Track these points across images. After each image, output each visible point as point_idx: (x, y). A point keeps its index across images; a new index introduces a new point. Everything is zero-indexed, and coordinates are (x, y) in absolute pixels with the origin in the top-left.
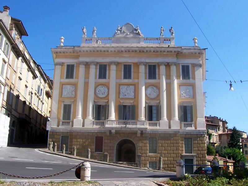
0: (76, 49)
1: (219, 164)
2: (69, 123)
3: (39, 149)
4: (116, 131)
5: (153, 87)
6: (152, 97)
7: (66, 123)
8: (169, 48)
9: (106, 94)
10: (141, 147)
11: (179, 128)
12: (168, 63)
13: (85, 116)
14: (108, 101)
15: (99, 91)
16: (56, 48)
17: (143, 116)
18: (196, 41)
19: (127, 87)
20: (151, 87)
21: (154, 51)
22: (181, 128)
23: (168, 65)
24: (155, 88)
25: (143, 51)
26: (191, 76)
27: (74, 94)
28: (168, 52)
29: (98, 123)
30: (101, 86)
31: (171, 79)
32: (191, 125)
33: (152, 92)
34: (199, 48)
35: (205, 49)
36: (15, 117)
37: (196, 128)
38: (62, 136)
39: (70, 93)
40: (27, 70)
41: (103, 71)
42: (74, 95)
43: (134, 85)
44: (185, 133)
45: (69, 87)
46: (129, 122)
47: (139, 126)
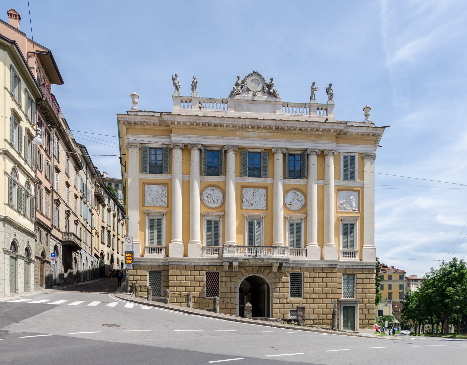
2: (161, 250)
5: (296, 192)
7: (156, 251)
13: (322, 244)
19: (254, 190)
20: (293, 191)
22: (339, 259)
23: (322, 155)
24: (299, 193)
28: (324, 130)
30: (211, 188)
33: (295, 200)
39: (159, 200)
44: (344, 267)
45: (155, 187)
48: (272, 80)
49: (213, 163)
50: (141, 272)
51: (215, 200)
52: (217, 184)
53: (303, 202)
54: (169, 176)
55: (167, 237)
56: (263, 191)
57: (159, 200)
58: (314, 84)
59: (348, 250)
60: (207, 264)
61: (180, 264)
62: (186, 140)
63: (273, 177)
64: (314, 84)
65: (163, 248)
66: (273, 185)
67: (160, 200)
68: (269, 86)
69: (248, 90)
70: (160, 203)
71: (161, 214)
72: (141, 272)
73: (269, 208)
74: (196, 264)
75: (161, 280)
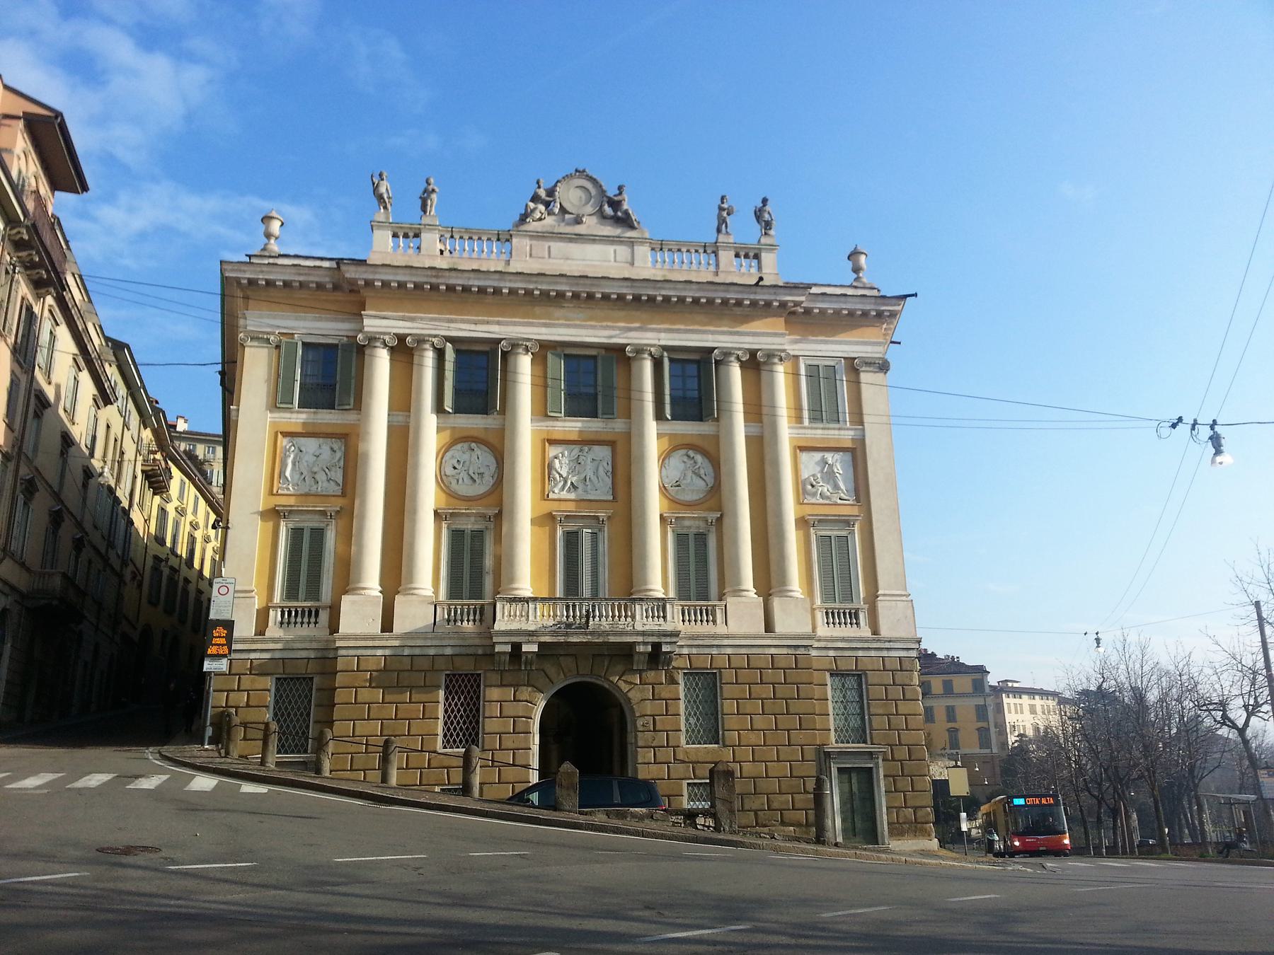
0: (351, 272)
3: (169, 750)
4: (541, 645)
5: (691, 453)
6: (689, 497)
8: (759, 289)
9: (488, 481)
11: (808, 629)
12: (401, 338)
14: (500, 512)
16: (247, 259)
17: (658, 575)
20: (683, 452)
21: (576, 296)
24: (699, 458)
26: (845, 406)
27: (340, 481)
29: (310, 612)
30: (466, 445)
32: (857, 617)
33: (690, 474)
34: (875, 293)
35: (906, 297)
36: (13, 588)
37: (875, 632)
38: (447, 675)
39: (321, 477)
40: (71, 361)
41: (477, 381)
43: (612, 444)
46: (574, 606)
47: (642, 621)
51: (475, 477)
52: (482, 435)
53: (710, 481)
54: (351, 417)
56: (603, 453)
57: (321, 477)
59: (843, 606)
60: (448, 651)
61: (369, 652)
62: (402, 327)
65: (324, 608)
67: (324, 478)
68: (615, 205)
71: (323, 513)
73: (620, 495)
74: (417, 651)
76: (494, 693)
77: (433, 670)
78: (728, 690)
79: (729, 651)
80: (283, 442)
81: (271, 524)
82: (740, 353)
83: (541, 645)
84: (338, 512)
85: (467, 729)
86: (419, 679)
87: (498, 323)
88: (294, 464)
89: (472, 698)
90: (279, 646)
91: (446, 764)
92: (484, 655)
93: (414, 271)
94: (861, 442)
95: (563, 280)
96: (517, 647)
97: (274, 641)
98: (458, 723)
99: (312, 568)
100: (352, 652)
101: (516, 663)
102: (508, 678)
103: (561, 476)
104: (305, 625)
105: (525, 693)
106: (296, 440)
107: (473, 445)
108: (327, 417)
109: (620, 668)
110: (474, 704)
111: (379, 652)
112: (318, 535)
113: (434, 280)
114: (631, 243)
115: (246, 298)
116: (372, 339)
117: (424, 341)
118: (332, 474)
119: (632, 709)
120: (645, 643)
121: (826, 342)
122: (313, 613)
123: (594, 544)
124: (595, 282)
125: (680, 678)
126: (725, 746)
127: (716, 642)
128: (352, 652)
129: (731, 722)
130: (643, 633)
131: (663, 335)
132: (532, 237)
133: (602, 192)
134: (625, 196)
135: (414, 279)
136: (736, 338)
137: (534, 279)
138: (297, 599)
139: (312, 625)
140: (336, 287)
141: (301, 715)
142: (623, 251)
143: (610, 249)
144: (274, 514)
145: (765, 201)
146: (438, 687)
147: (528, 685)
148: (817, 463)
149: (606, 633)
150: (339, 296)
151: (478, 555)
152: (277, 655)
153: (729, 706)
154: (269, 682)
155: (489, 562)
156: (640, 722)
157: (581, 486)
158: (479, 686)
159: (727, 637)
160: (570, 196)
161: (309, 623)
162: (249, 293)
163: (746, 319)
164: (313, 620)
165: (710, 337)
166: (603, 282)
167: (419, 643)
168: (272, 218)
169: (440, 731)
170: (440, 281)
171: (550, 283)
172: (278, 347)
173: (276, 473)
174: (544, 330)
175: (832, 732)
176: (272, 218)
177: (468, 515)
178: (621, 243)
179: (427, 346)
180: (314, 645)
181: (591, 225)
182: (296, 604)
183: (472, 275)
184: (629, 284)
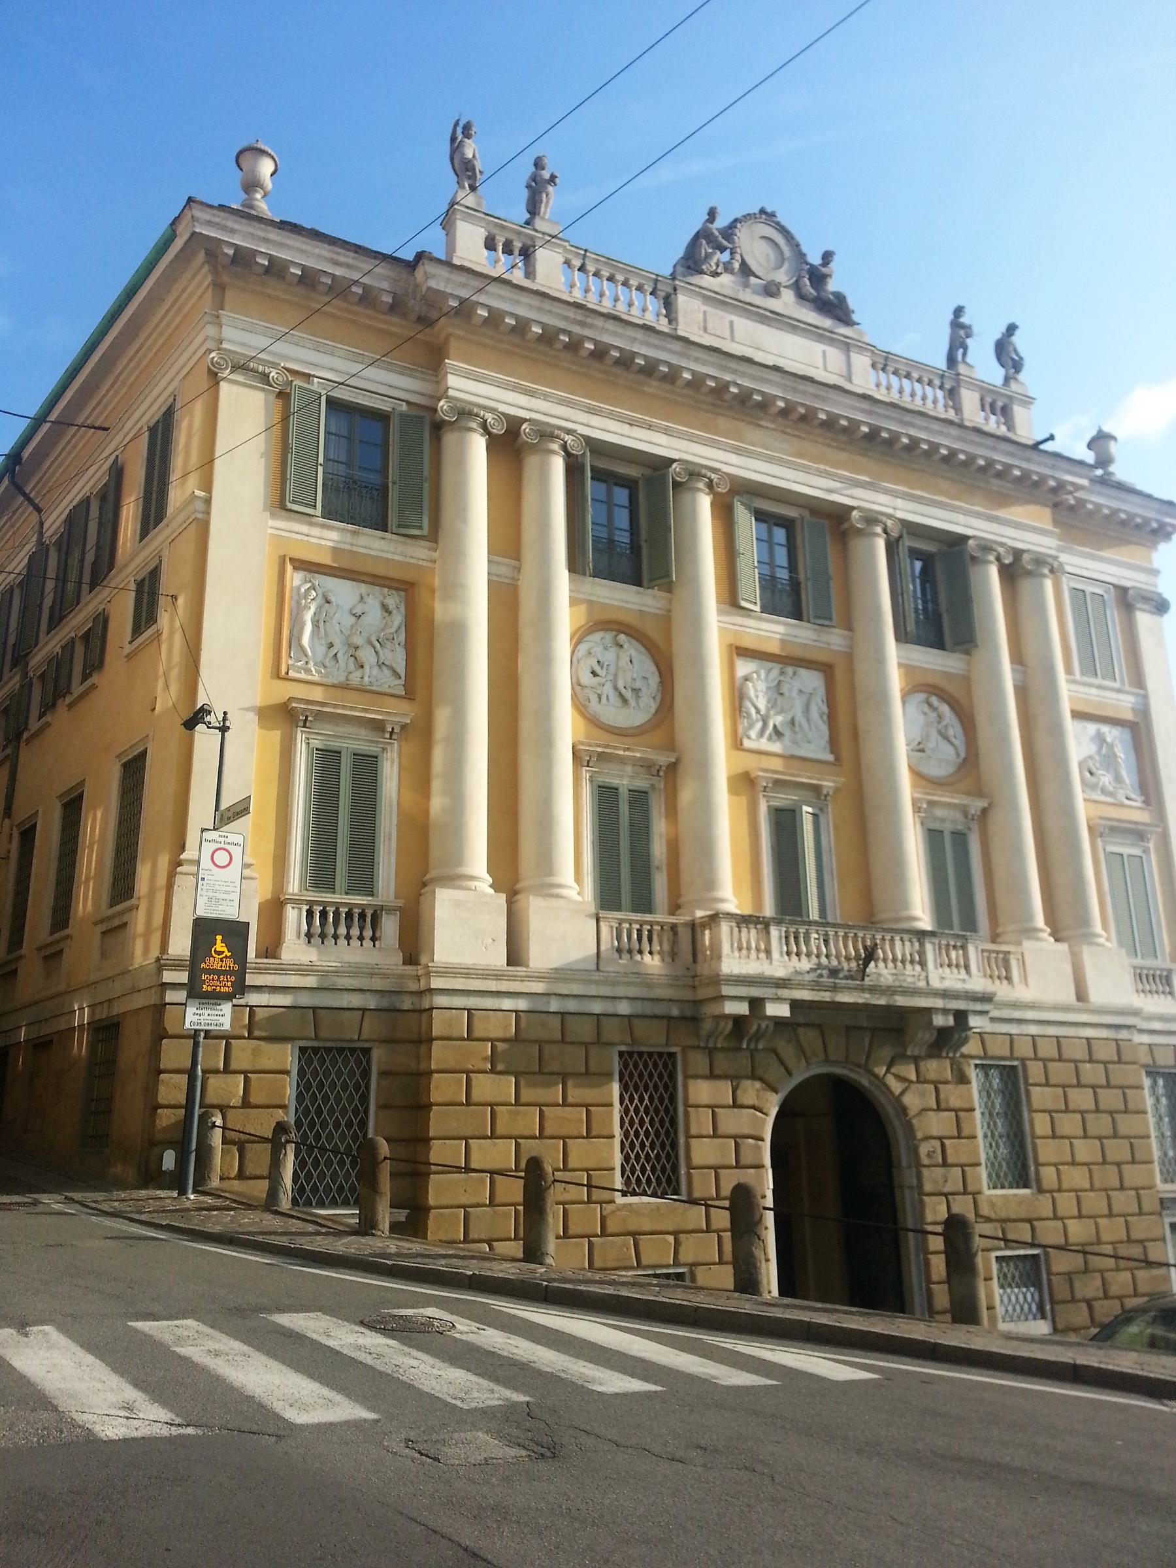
1: (522, 1181)
4: (795, 1004)
5: (934, 700)
8: (1034, 455)
10: (937, 1144)
12: (514, 425)
13: (512, 872)
15: (594, 673)
18: (266, 167)
19: (782, 673)
24: (945, 709)
25: (574, 346)
27: (401, 670)
29: (362, 916)
30: (609, 636)
31: (441, 541)
33: (934, 736)
38: (621, 1054)
42: (396, 674)
48: (827, 257)
49: (628, 525)
50: (256, 1053)
51: (628, 694)
52: (634, 621)
54: (418, 552)
55: (955, 852)
58: (959, 311)
60: (624, 1008)
61: (489, 1003)
63: (849, 627)
64: (959, 311)
65: (391, 910)
66: (849, 657)
67: (373, 659)
68: (818, 277)
69: (746, 271)
70: (372, 676)
71: (378, 726)
72: (256, 1053)
73: (846, 754)
74: (572, 1006)
75: (364, 1099)
76: (702, 1091)
77: (599, 1041)
78: (1041, 1096)
79: (1033, 1030)
80: (295, 579)
81: (276, 736)
82: (1001, 550)
83: (795, 1004)
84: (404, 727)
85: (658, 1157)
86: (574, 1059)
87: (666, 432)
88: (316, 624)
89: (661, 1100)
90: (310, 981)
91: (632, 1227)
92: (683, 1018)
93: (547, 305)
94: (1144, 712)
95: (775, 377)
96: (756, 1004)
97: (301, 970)
98: (642, 1146)
99: (358, 833)
100: (459, 1001)
101: (744, 1041)
102: (723, 1063)
103: (758, 711)
104: (355, 943)
105: (751, 1091)
106: (319, 579)
107: (622, 637)
108: (374, 545)
109: (886, 1052)
110: (667, 1111)
111: (507, 1004)
112: (367, 766)
113: (577, 329)
114: (846, 346)
115: (219, 288)
116: (465, 413)
117: (552, 437)
118: (386, 655)
119: (910, 1129)
120: (945, 1011)
121: (1093, 558)
122: (367, 922)
123: (817, 831)
124: (821, 392)
125: (973, 1074)
126: (1041, 1190)
127: (1017, 1014)
128: (459, 1001)
129: (1047, 1151)
130: (945, 994)
131: (899, 503)
132: (707, 300)
133: (801, 256)
134: (834, 265)
135: (545, 319)
136: (994, 527)
137: (734, 365)
138: (332, 889)
139: (368, 943)
140: (396, 308)
141: (349, 1125)
142: (835, 355)
143: (819, 348)
144: (286, 716)
145: (1011, 329)
146: (609, 1075)
147: (753, 1077)
148: (1092, 739)
149: (890, 991)
150: (395, 324)
151: (641, 832)
152: (305, 1000)
153: (1041, 1124)
154: (287, 1056)
155: (659, 850)
156: (923, 1149)
157: (788, 733)
158: (672, 1076)
159: (1032, 1006)
160: (753, 246)
161: (361, 938)
162: (226, 278)
163: (1004, 500)
164: (368, 933)
165: (961, 518)
166: (832, 395)
167: (577, 989)
168: (263, 152)
169: (617, 1159)
170: (587, 332)
171: (754, 378)
172: (283, 396)
173: (283, 639)
174: (733, 458)
175: (1156, 1164)
176: (263, 152)
177: (622, 760)
178: (832, 342)
179: (555, 447)
180: (377, 984)
181: (786, 303)
182: (327, 897)
183: (640, 335)
184: (865, 405)
